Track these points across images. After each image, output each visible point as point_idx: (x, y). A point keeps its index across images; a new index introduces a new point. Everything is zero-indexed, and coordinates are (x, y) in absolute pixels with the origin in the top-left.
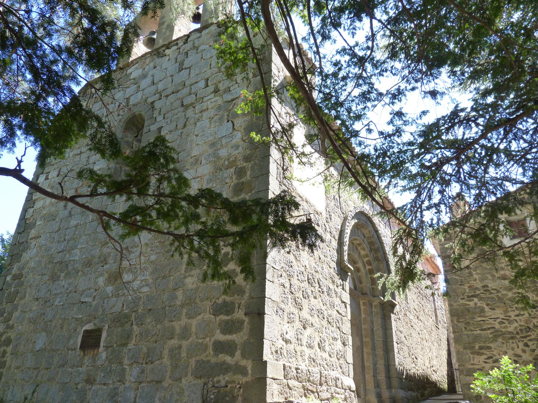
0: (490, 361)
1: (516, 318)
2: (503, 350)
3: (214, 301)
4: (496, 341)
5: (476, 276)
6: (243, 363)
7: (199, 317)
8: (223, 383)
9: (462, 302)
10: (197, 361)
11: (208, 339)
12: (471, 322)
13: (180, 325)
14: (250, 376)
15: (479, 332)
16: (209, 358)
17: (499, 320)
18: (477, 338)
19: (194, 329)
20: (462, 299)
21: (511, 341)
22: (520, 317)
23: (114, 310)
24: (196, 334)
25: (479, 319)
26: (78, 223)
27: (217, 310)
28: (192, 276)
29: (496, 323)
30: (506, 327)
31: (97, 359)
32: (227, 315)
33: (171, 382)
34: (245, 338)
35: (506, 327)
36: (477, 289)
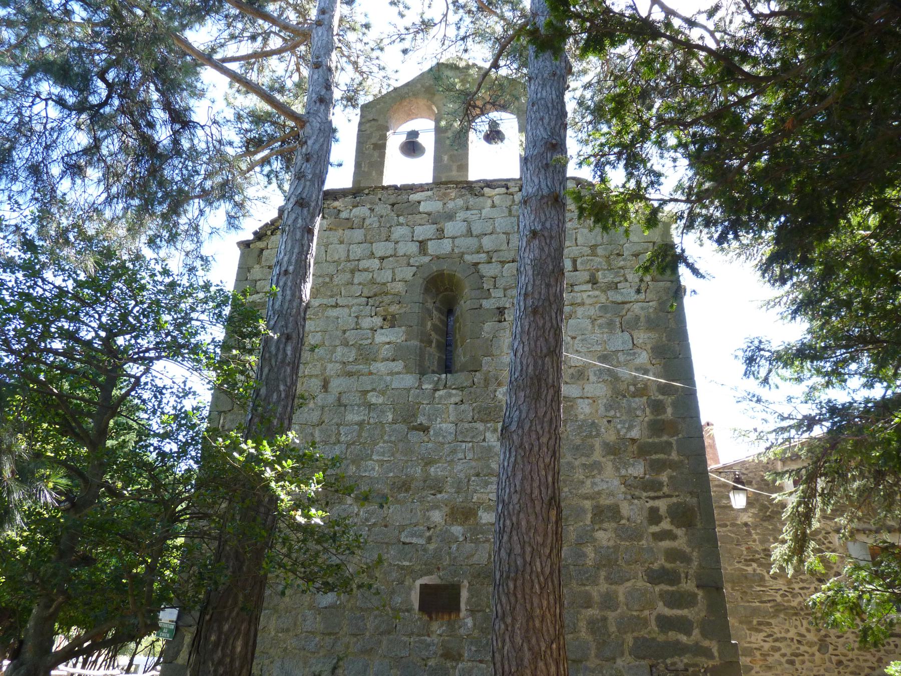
0: (770, 639)
1: (801, 591)
2: (785, 627)
3: (646, 565)
4: (778, 616)
5: (755, 536)
6: (706, 643)
7: (629, 584)
8: (681, 666)
9: (738, 565)
10: (636, 639)
11: (646, 612)
12: (749, 591)
13: (599, 591)
14: (717, 659)
15: (758, 604)
16: (654, 636)
17: (781, 592)
18: (755, 611)
19: (621, 598)
20: (738, 562)
21: (794, 618)
22: (805, 591)
23: (475, 560)
24: (627, 605)
25: (759, 589)
26: (364, 420)
27: (655, 577)
28: (605, 530)
29: (778, 595)
30: (789, 601)
31: (457, 626)
32: (672, 585)
33: (598, 662)
34: (703, 614)
35: (789, 601)
36: (756, 552)
